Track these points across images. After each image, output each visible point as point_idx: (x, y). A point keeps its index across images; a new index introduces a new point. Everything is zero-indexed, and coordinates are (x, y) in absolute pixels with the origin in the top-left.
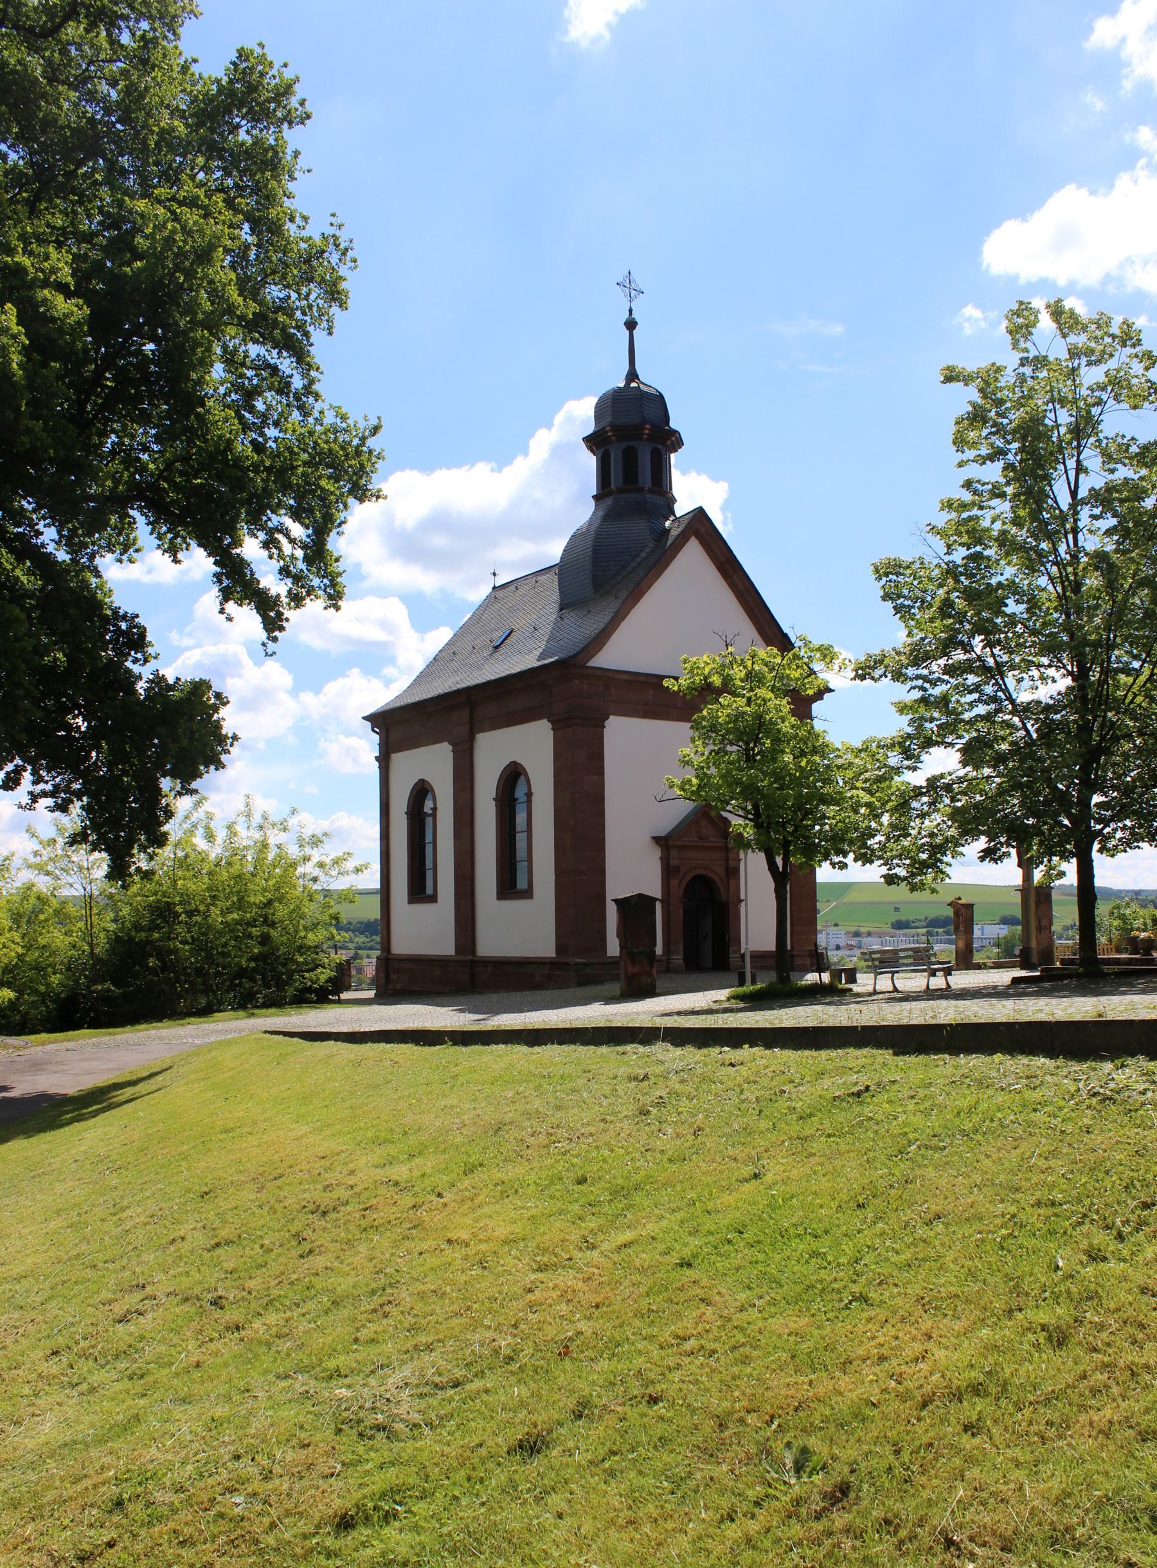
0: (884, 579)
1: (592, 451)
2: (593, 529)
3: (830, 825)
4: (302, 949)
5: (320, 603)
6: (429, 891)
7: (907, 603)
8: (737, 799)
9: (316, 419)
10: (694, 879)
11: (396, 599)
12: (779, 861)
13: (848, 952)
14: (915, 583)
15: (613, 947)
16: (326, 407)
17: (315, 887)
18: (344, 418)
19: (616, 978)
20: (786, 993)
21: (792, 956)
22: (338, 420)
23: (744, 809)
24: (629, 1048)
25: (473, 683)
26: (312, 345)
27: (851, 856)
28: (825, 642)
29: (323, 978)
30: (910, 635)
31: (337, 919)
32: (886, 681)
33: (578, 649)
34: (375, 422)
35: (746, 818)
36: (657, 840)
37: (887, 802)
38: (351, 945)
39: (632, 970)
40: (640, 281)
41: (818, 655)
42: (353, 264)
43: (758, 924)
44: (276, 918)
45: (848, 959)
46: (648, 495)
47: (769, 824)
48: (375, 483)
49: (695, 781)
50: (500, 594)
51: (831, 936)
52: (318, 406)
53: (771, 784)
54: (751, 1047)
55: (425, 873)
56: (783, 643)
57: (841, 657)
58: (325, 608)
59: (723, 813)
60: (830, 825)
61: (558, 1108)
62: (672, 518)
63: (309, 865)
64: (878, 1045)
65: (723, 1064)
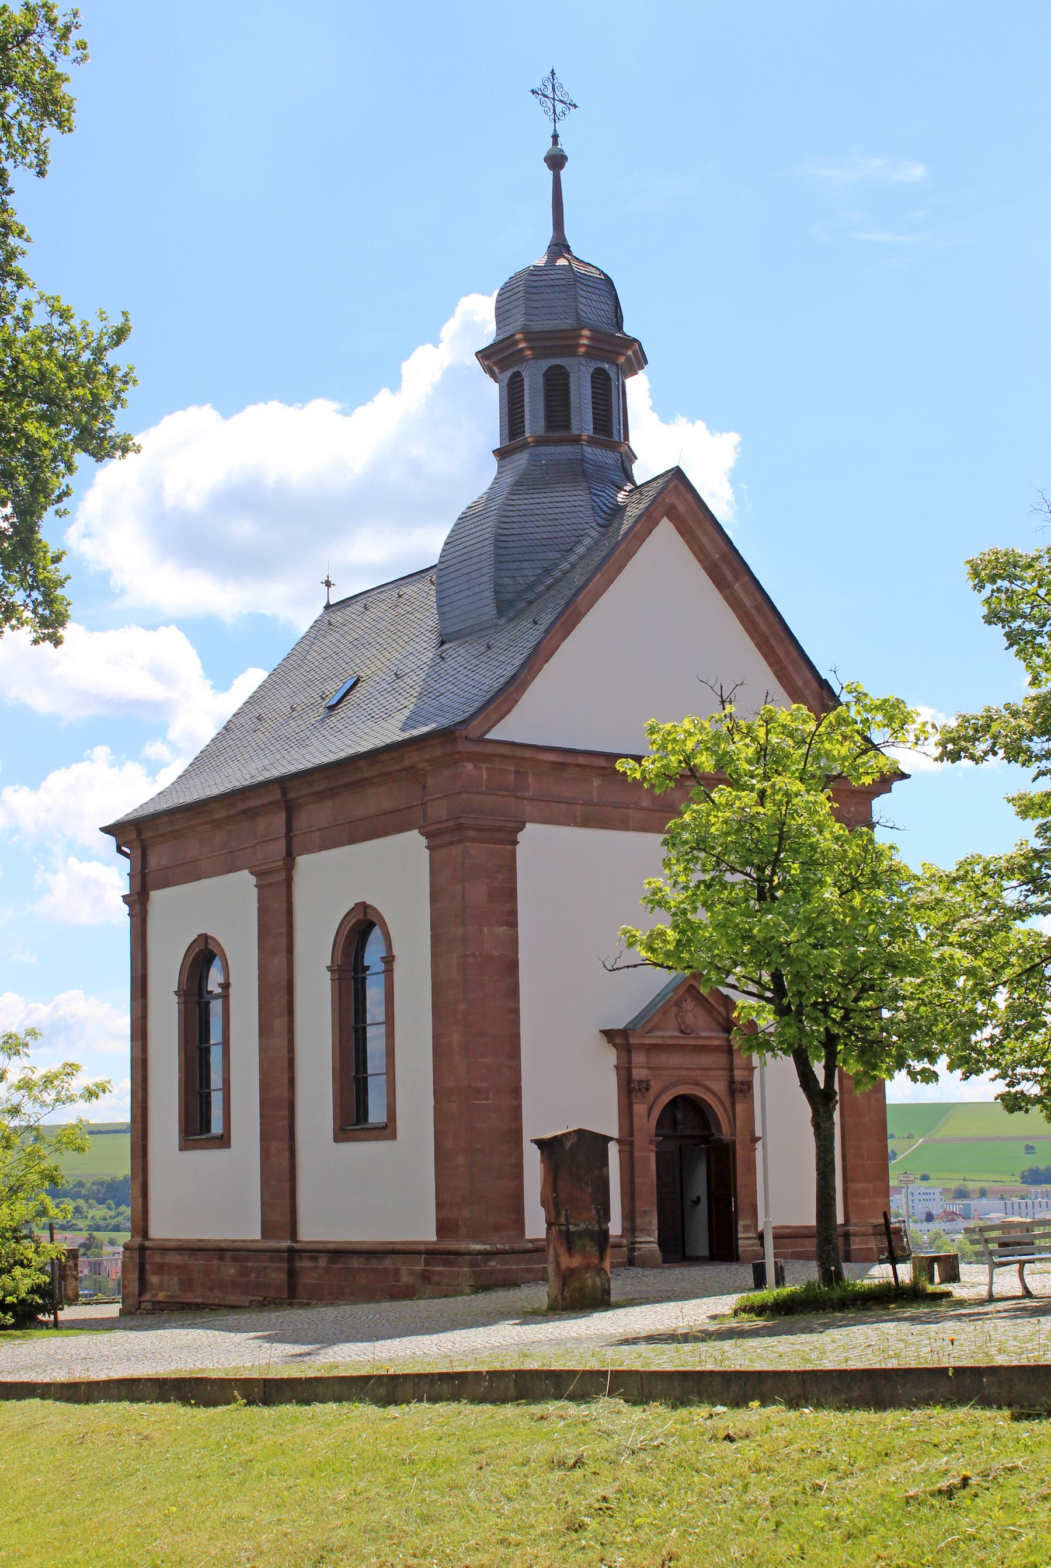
0: (989, 587)
1: (493, 375)
2: (495, 505)
3: (907, 1011)
5: (26, 634)
6: (217, 1128)
7: (1028, 626)
8: (743, 964)
9: (18, 319)
10: (674, 1102)
11: (173, 628)
12: (818, 1069)
13: (947, 1226)
14: (1042, 592)
15: (536, 1225)
16: (34, 297)
17: (15, 1123)
18: (65, 315)
19: (542, 1277)
20: (832, 1302)
21: (847, 1235)
22: (56, 320)
23: (758, 982)
24: (551, 1407)
25: (292, 768)
26: (10, 192)
27: (943, 1060)
28: (892, 695)
30: (1035, 681)
31: (52, 1179)
32: (997, 762)
33: (471, 710)
34: (117, 321)
35: (760, 997)
36: (609, 1035)
37: (1003, 967)
38: (81, 1223)
39: (566, 1262)
40: (570, 86)
41: (879, 717)
42: (78, 53)
43: (783, 1185)
45: (946, 1238)
46: (588, 449)
47: (800, 1006)
48: (120, 423)
49: (671, 935)
50: (338, 617)
51: (917, 1197)
52: (24, 295)
53: (802, 939)
54: (763, 1405)
55: (208, 1095)
56: (821, 696)
57: (920, 720)
58: (35, 642)
59: (721, 988)
60: (907, 1011)
61: (426, 1519)
62: (629, 487)
64: (986, 1402)
65: (714, 1438)
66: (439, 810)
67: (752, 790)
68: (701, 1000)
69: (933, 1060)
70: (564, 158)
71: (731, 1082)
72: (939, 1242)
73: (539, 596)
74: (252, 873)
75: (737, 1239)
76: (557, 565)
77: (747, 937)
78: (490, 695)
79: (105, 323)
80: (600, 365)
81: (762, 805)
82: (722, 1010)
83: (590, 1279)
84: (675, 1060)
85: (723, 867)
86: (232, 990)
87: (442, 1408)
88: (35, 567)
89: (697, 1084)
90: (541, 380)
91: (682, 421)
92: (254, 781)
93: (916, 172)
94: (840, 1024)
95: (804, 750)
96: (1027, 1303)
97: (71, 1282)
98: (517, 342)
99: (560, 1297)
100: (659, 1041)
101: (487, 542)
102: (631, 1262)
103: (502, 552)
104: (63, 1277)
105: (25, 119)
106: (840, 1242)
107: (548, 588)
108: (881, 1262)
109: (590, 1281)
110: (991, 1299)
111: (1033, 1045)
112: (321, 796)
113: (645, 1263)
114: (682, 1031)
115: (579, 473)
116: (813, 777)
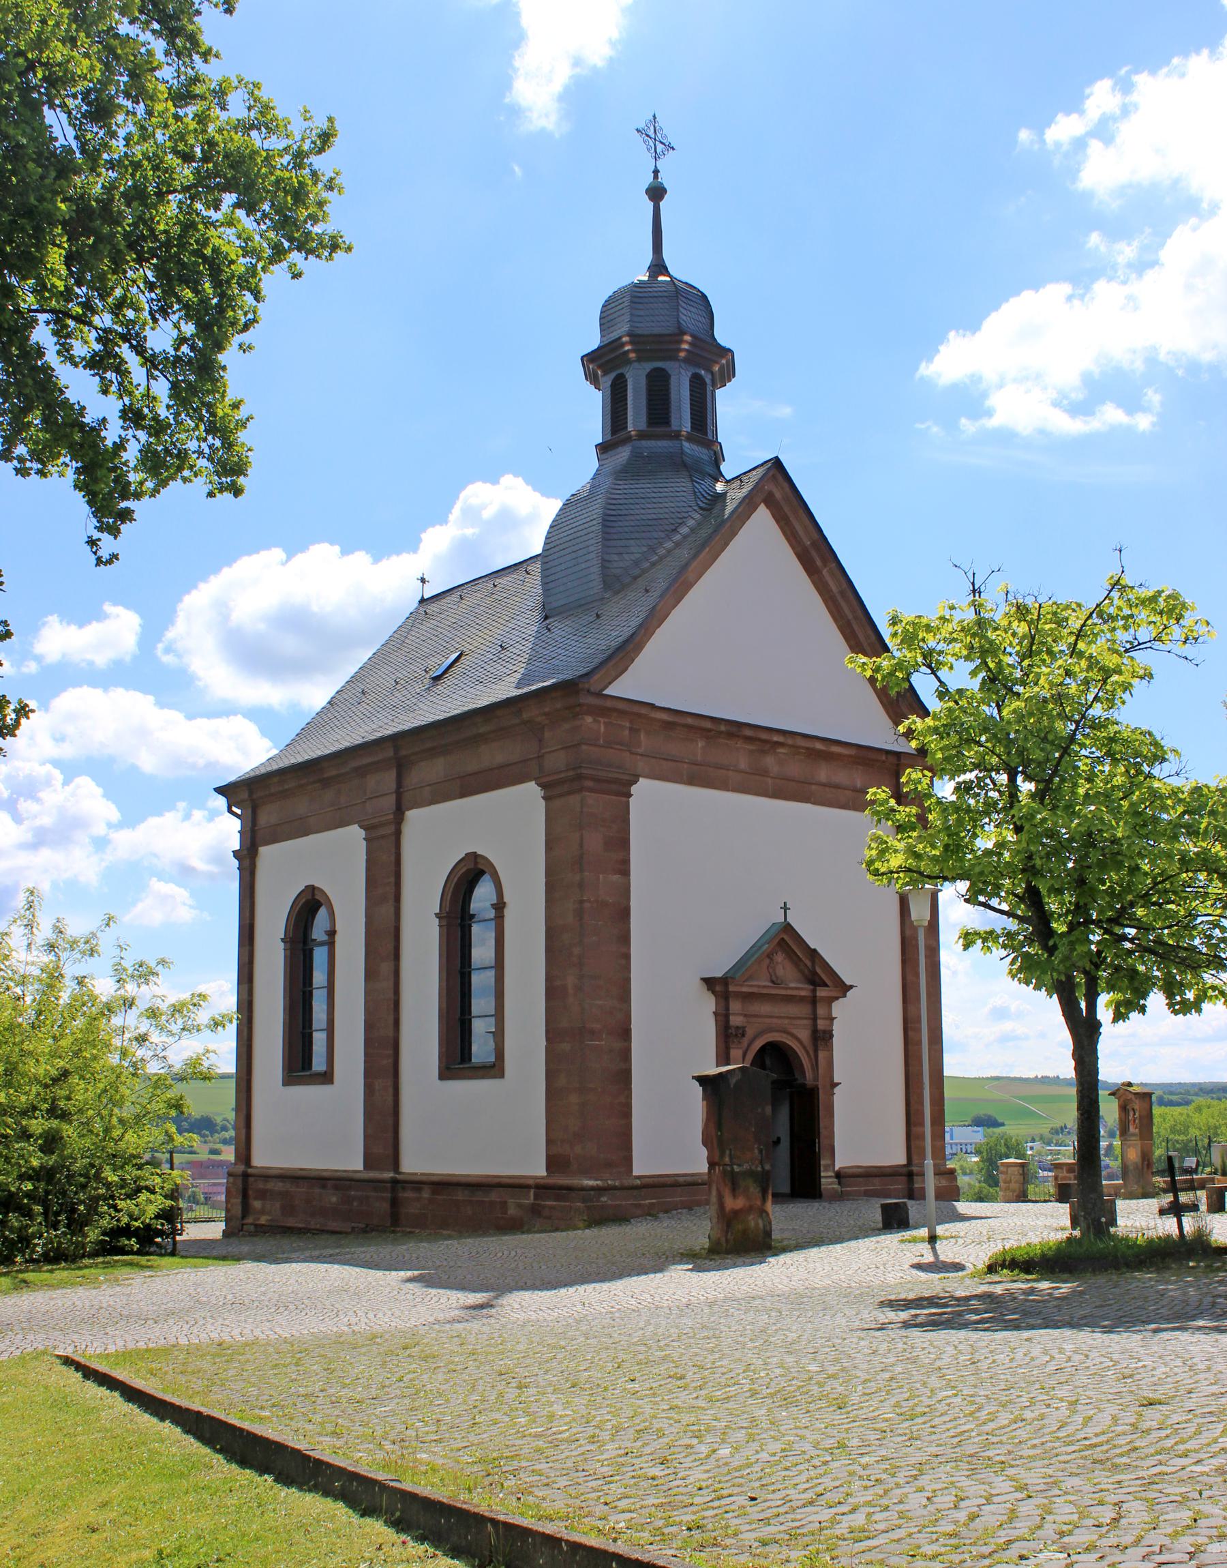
4: (119, 1160)
10: (763, 1049)
29: (151, 1210)
34: (321, 123)
36: (709, 983)
39: (731, 1203)
44: (71, 1106)
46: (686, 444)
50: (433, 608)
58: (211, 494)
63: (133, 1014)
66: (557, 761)
70: (664, 191)
74: (361, 827)
75: (820, 1177)
76: (661, 544)
78: (609, 652)
79: (309, 124)
82: (809, 964)
83: (753, 1222)
84: (765, 1008)
86: (338, 938)
90: (643, 382)
98: (623, 345)
99: (723, 1240)
100: (755, 990)
101: (594, 522)
103: (608, 530)
107: (654, 564)
109: (752, 1224)
112: (433, 753)
114: (773, 982)
115: (681, 465)
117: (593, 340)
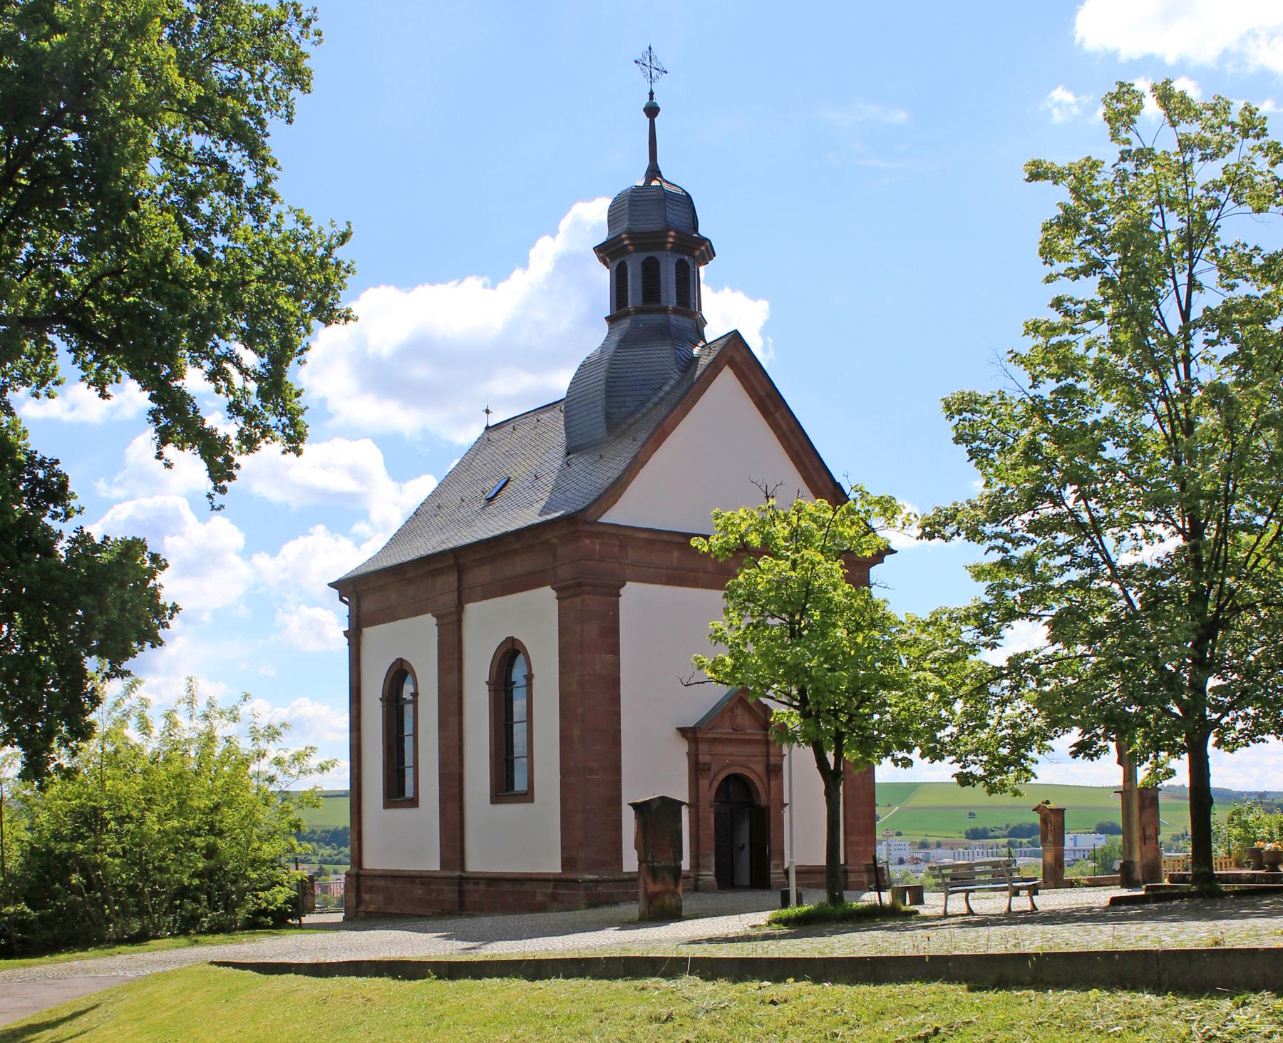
0: (957, 417)
1: (605, 263)
2: (606, 357)
5: (277, 447)
6: (409, 793)
7: (984, 446)
9: (273, 225)
10: (728, 778)
11: (369, 441)
12: (830, 757)
13: (913, 867)
15: (631, 862)
16: (284, 209)
17: (271, 789)
18: (306, 223)
19: (633, 898)
21: (846, 872)
22: (300, 226)
23: (788, 694)
24: (649, 982)
27: (917, 751)
28: (886, 494)
29: (281, 898)
31: (298, 827)
32: (959, 540)
33: (588, 502)
34: (343, 228)
35: (790, 705)
36: (683, 731)
38: (314, 859)
39: (654, 888)
40: (662, 59)
41: (877, 509)
43: (804, 837)
44: (224, 826)
46: (672, 317)
47: (818, 712)
49: (729, 661)
50: (494, 435)
51: (893, 847)
53: (820, 664)
54: (796, 981)
56: (836, 495)
57: (905, 512)
58: (284, 453)
59: (762, 699)
63: (264, 761)
64: (950, 979)
65: (763, 1002)
66: (565, 572)
67: (787, 558)
68: (748, 708)
69: (910, 752)
71: (768, 765)
72: (907, 879)
73: (637, 421)
77: (781, 662)
80: (682, 257)
81: (794, 570)
82: (762, 715)
83: (668, 900)
84: (728, 749)
85: (766, 613)
86: (419, 698)
87: (573, 982)
88: (284, 400)
89: (729, 766)
90: (640, 267)
91: (727, 290)
92: (435, 551)
93: (901, 117)
94: (846, 724)
95: (824, 531)
96: (970, 918)
97: (309, 897)
98: (623, 240)
102: (696, 889)
104: (305, 894)
105: (278, 83)
106: (842, 876)
107: (644, 415)
108: (871, 890)
110: (946, 915)
111: (980, 741)
113: (706, 890)
115: (664, 333)
116: (830, 551)
117: (603, 236)
